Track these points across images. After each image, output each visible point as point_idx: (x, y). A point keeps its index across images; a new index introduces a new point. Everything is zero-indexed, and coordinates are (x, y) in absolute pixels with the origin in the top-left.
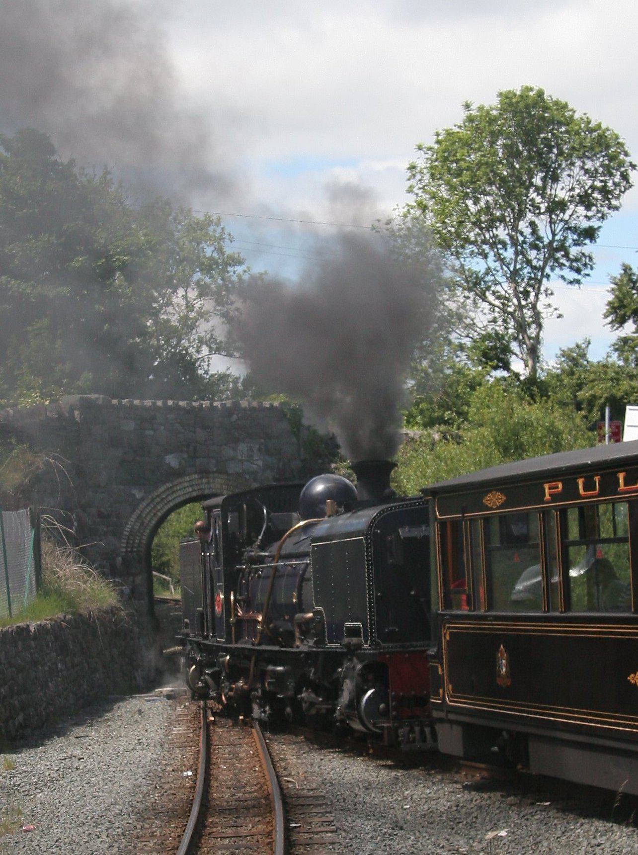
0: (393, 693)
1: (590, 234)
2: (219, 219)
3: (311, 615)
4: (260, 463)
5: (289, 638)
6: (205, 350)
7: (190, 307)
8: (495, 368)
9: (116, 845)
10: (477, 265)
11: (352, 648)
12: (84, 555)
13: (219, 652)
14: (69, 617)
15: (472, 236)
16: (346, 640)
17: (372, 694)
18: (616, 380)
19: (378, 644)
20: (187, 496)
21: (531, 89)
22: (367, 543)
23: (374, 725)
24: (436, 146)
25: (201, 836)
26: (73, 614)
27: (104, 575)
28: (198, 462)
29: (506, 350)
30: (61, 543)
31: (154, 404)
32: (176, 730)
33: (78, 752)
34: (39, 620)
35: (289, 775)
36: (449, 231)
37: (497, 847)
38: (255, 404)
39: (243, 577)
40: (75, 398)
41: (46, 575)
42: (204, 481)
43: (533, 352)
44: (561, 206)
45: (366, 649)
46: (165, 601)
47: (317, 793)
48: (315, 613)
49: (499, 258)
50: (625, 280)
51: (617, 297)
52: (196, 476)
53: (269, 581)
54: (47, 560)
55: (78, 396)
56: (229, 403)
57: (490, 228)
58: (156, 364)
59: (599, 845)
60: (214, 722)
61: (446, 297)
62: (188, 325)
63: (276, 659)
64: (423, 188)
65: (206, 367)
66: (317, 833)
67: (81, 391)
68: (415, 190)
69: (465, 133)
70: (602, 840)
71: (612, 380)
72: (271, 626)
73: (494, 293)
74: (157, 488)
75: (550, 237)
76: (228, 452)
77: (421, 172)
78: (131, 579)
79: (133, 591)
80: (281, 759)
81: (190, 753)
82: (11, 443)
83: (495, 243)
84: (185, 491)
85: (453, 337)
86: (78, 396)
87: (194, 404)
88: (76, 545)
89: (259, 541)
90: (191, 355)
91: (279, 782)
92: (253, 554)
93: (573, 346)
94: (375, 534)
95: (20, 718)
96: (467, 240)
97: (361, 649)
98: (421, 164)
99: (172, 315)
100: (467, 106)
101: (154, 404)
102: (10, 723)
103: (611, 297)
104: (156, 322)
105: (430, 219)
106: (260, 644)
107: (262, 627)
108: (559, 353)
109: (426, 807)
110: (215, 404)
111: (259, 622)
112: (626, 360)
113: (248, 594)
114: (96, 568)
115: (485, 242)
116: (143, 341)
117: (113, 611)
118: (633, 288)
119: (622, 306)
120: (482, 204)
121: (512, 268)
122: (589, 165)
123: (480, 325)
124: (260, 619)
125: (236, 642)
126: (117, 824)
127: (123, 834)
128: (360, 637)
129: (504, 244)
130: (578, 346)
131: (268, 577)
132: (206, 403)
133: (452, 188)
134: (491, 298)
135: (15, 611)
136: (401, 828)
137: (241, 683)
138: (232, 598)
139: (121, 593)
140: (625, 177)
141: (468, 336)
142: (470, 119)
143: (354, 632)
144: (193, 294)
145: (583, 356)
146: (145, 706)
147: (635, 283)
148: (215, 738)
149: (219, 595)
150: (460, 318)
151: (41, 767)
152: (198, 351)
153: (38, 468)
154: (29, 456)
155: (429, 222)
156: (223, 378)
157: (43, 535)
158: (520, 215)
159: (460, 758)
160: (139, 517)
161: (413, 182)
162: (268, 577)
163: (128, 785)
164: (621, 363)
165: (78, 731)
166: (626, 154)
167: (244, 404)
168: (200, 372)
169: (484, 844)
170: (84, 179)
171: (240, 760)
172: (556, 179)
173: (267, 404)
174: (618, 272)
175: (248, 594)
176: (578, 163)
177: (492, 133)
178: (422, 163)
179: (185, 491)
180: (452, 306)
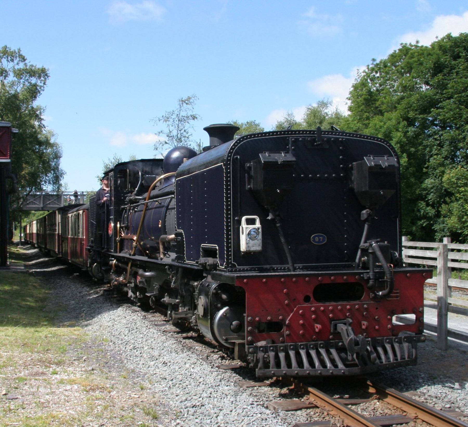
0: (249, 318)
3: (173, 236)
5: (155, 250)
11: (208, 268)
13: (110, 258)
16: (202, 260)
19: (234, 266)
22: (227, 169)
23: (226, 340)
39: (126, 212)
45: (220, 270)
48: (177, 235)
53: (143, 212)
63: (145, 266)
72: (142, 243)
89: (136, 191)
92: (132, 197)
94: (235, 160)
97: (216, 270)
106: (134, 255)
107: (136, 243)
111: (134, 240)
113: (128, 223)
124: (135, 238)
125: (120, 252)
128: (217, 258)
131: (142, 211)
137: (121, 279)
138: (118, 226)
143: (210, 253)
149: (111, 223)
159: (371, 386)
162: (142, 211)
175: (128, 223)
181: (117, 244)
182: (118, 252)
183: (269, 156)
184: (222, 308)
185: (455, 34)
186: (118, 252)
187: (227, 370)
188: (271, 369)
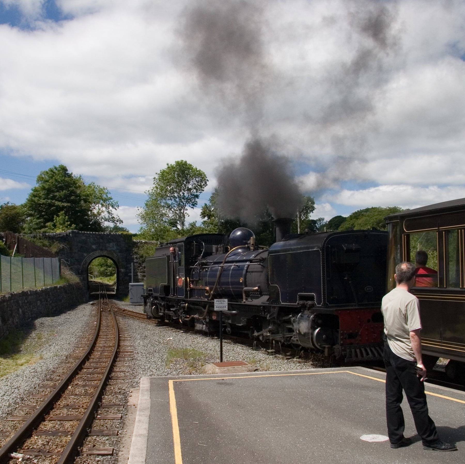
0: (342, 332)
1: (197, 196)
2: (107, 188)
3: (257, 288)
4: (115, 248)
6: (103, 220)
7: (99, 209)
8: (174, 227)
9: (77, 339)
10: (170, 202)
12: (71, 269)
14: (67, 284)
15: (169, 195)
17: (319, 330)
18: (203, 231)
20: (97, 256)
21: (183, 161)
23: (320, 346)
24: (160, 173)
25: (98, 338)
26: (68, 283)
27: (76, 274)
28: (100, 247)
29: (176, 223)
30: (66, 266)
31: (90, 233)
32: (93, 312)
33: (69, 317)
34: (60, 284)
35: (120, 324)
36: (163, 194)
37: (170, 342)
38: (115, 233)
40: (70, 231)
41: (62, 273)
42: (102, 252)
43: (183, 224)
44: (190, 189)
46: (91, 281)
47: (127, 328)
49: (175, 200)
50: (205, 207)
51: (203, 211)
52: (99, 251)
54: (62, 270)
55: (71, 230)
56: (108, 233)
57: (173, 193)
58: (91, 223)
59: (194, 341)
60: (102, 311)
61: (162, 209)
62: (99, 214)
64: (157, 183)
65: (103, 224)
66: (126, 338)
67: (72, 229)
68: (155, 183)
69: (167, 171)
70: (195, 340)
71: (201, 231)
73: (174, 209)
74: (90, 253)
75: (188, 196)
76: (107, 245)
77: (157, 179)
78: (83, 276)
79: (83, 278)
80: (118, 320)
81: (96, 318)
82: (54, 241)
83: (174, 197)
84: (97, 254)
85: (164, 219)
86: (71, 230)
87: (100, 233)
88: (70, 267)
90: (100, 221)
91: (118, 326)
93: (192, 222)
95: (55, 309)
96: (167, 196)
97: (314, 307)
98: (157, 177)
99: (95, 211)
100: (168, 165)
101: (90, 233)
102: (52, 310)
103: (202, 211)
104: (91, 213)
105: (159, 191)
108: (189, 224)
109: (153, 332)
110: (105, 233)
112: (205, 226)
114: (74, 273)
115: (172, 196)
116: (88, 218)
117: (78, 283)
118: (207, 209)
119: (204, 213)
120: (171, 187)
121: (178, 203)
122: (197, 179)
123: (170, 216)
125: (190, 298)
126: (77, 335)
127: (79, 337)
129: (176, 198)
130: (194, 222)
132: (103, 233)
133: (164, 184)
134: (172, 209)
135: (54, 283)
136: (147, 337)
139: (80, 279)
140: (206, 183)
141: (167, 219)
142: (169, 167)
144: (100, 206)
145: (195, 225)
146: (86, 307)
147: (207, 208)
148: (102, 315)
150: (165, 214)
151: (59, 321)
152: (101, 220)
153: (61, 247)
154: (59, 245)
155: (158, 191)
156: (107, 227)
157: (61, 264)
158: (180, 191)
160: (85, 260)
161: (155, 182)
163: (80, 325)
164: (204, 227)
165: (69, 312)
166: (206, 177)
167: (112, 233)
168: (102, 225)
169: (167, 341)
170: (75, 178)
171: (108, 320)
172: (189, 183)
173: (117, 234)
174: (204, 205)
176: (195, 179)
177: (174, 171)
178: (157, 177)
179: (97, 254)
180: (164, 212)
181: (188, 293)
182: (188, 298)
183: (347, 245)
184: (317, 329)
185: (362, 209)
186: (188, 298)
187: (66, 422)
188: (353, 358)
